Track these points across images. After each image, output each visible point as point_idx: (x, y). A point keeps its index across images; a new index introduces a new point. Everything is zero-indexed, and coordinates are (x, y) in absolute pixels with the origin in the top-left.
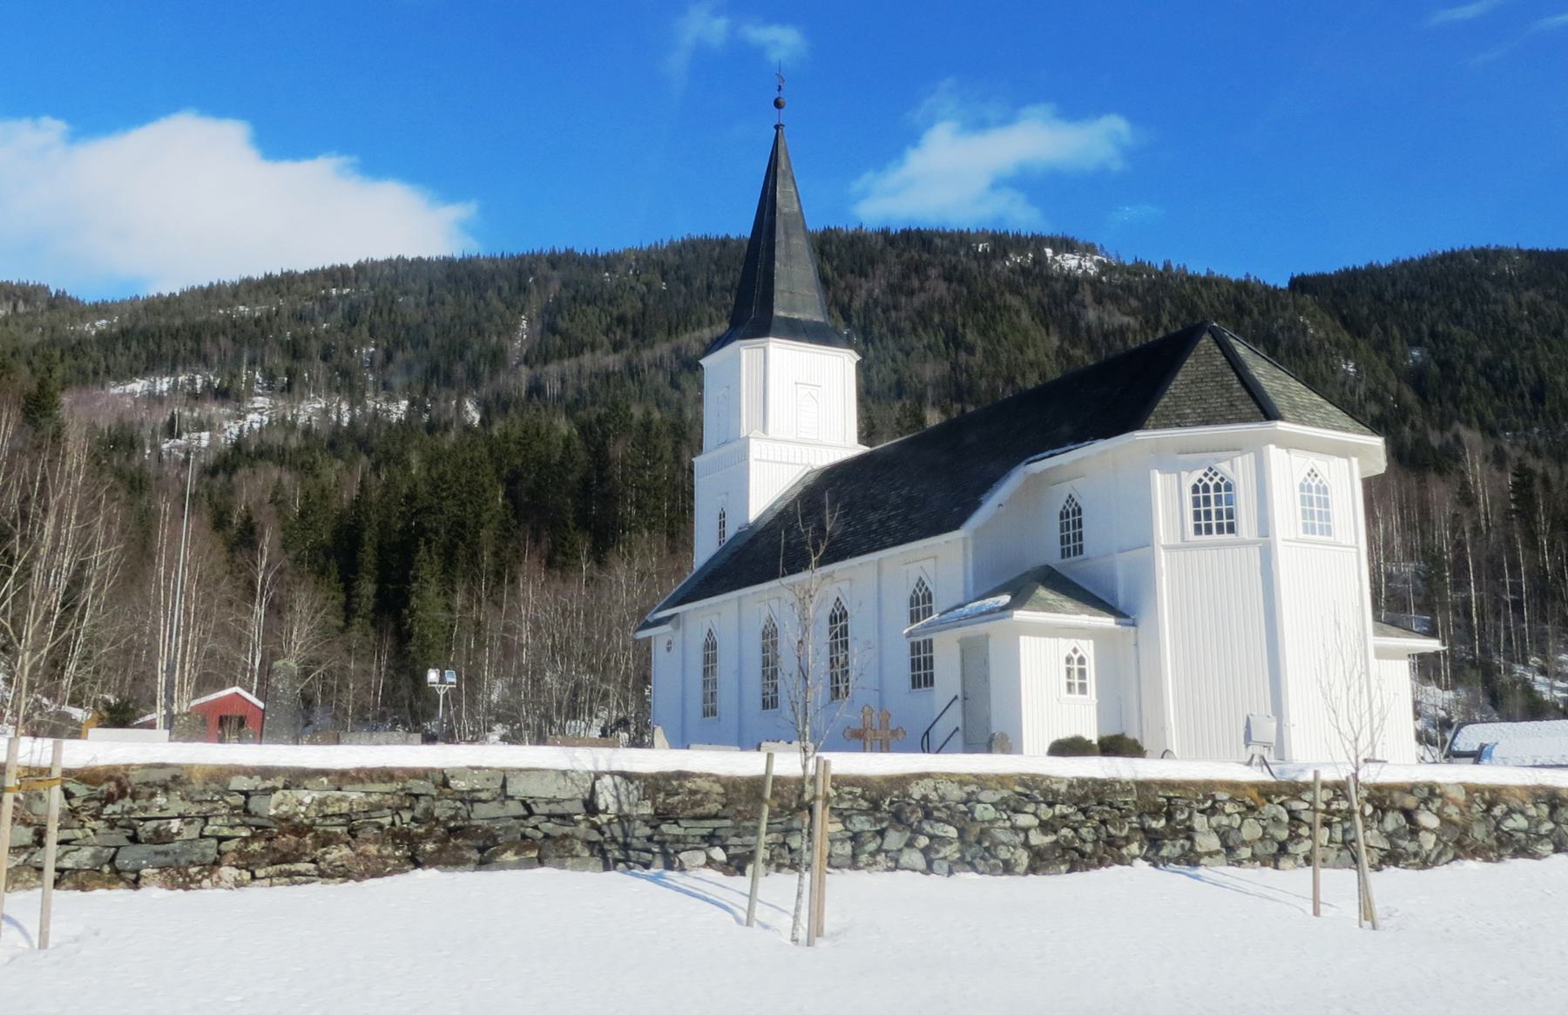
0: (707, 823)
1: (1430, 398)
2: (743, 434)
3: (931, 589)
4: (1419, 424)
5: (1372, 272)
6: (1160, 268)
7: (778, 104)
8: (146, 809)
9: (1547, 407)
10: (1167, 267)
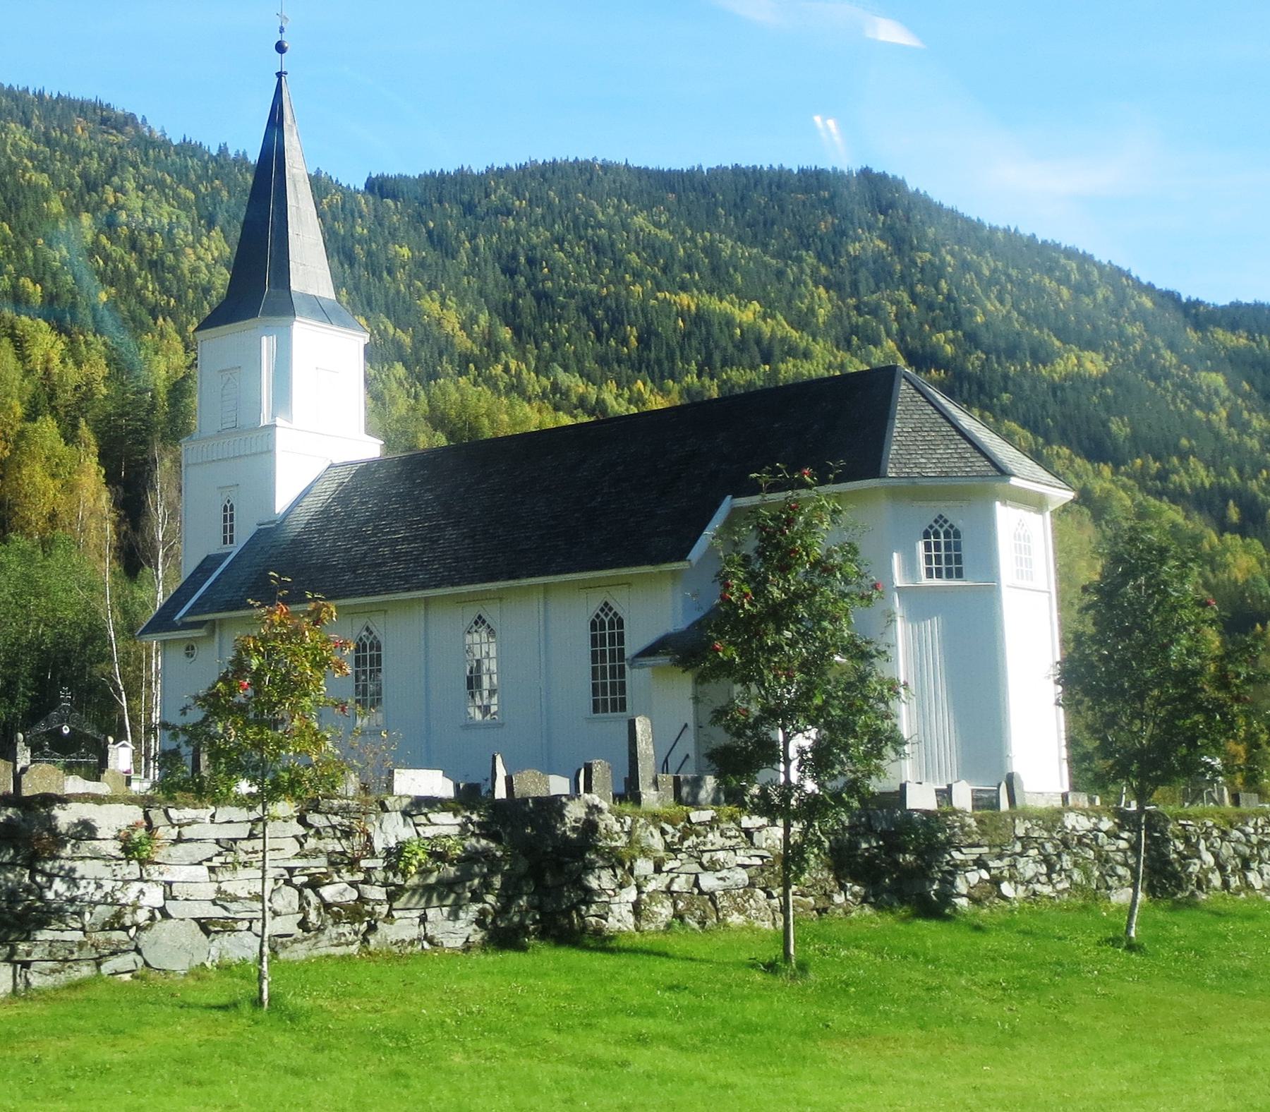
0: (975, 850)
1: (524, 335)
2: (265, 420)
3: (620, 613)
4: (513, 365)
5: (462, 179)
6: (214, 152)
7: (280, 48)
8: (705, 844)
9: (653, 355)
10: (223, 150)
